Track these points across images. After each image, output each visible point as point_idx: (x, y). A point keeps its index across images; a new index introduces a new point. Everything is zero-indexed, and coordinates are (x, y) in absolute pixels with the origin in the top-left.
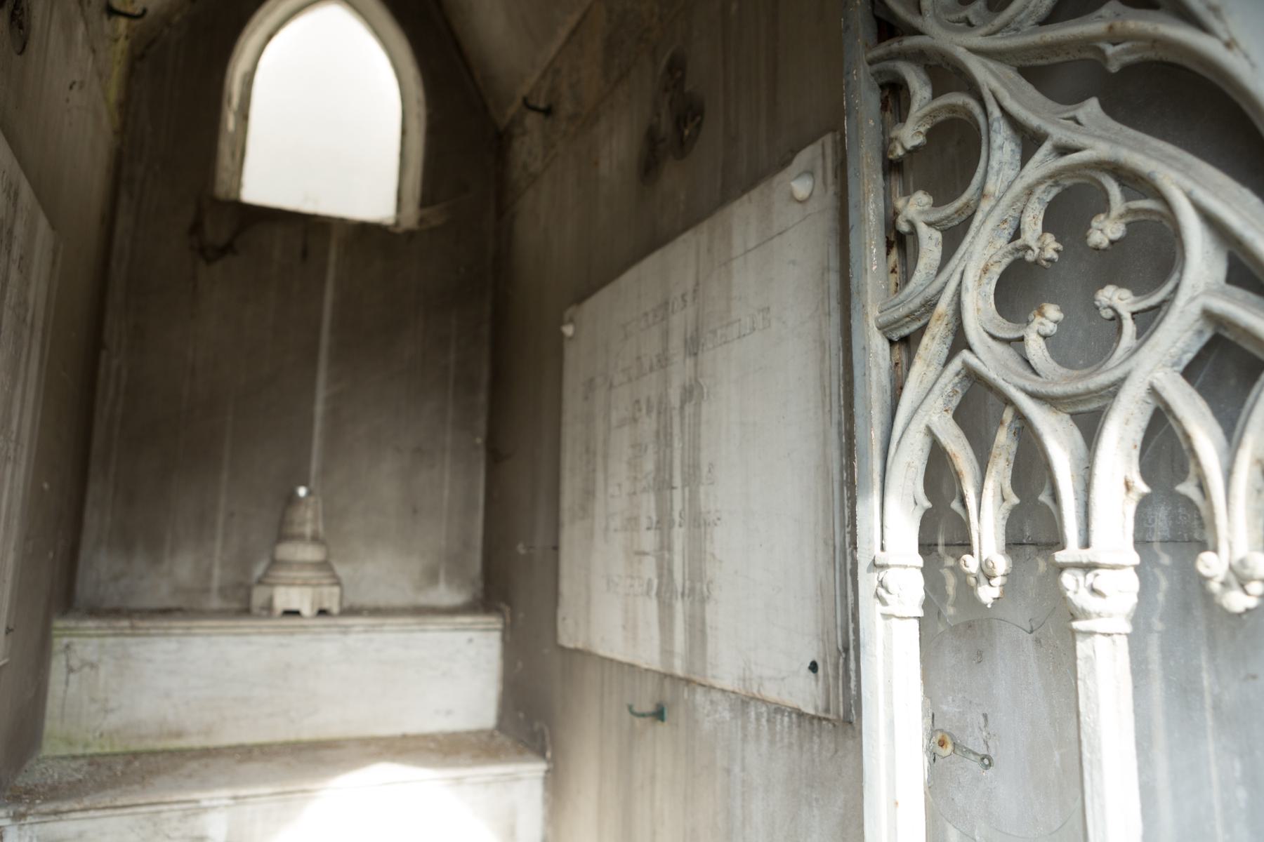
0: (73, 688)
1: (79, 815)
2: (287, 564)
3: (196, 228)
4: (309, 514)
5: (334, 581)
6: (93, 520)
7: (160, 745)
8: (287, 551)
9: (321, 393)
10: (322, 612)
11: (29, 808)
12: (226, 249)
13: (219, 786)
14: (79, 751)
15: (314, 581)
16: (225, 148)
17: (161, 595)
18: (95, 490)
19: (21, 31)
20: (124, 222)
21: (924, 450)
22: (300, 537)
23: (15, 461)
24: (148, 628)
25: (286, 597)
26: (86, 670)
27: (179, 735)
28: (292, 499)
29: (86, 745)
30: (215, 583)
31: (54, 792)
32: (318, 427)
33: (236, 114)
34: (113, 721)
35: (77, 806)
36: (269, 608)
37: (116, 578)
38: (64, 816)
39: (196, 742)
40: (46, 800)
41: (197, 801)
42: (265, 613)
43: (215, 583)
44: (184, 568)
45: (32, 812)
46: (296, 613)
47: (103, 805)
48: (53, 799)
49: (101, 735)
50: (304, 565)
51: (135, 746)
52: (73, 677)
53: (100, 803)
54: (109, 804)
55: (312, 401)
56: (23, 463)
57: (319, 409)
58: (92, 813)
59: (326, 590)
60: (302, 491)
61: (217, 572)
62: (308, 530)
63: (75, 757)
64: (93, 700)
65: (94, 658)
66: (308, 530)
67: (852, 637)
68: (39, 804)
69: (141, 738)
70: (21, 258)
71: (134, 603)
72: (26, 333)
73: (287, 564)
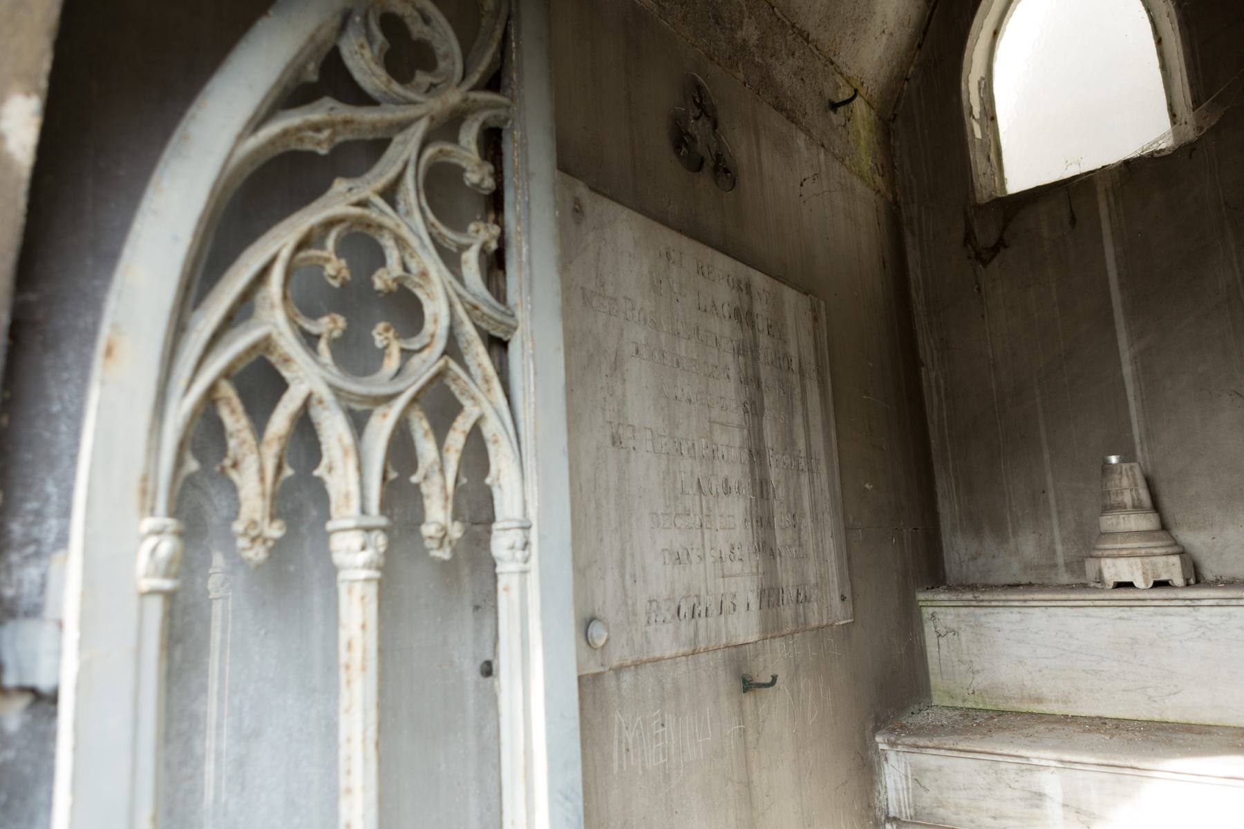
0: (944, 651)
1: (933, 751)
2: (1111, 535)
3: (969, 238)
4: (1125, 482)
5: (1176, 549)
6: (947, 510)
7: (1024, 708)
8: (1109, 522)
9: (1126, 354)
10: (1159, 584)
11: (897, 739)
12: (1000, 244)
13: (1045, 747)
14: (959, 704)
15: (1143, 552)
16: (977, 157)
17: (1014, 572)
18: (943, 485)
19: (729, 174)
20: (913, 257)
21: (465, 345)
22: (1121, 507)
23: (810, 471)
24: (990, 601)
25: (1116, 569)
26: (950, 635)
27: (1039, 700)
28: (1106, 469)
29: (964, 701)
30: (1060, 560)
31: (935, 730)
32: (1130, 390)
33: (980, 121)
34: (980, 681)
35: (929, 744)
36: (1100, 579)
37: (974, 559)
38: (924, 751)
39: (1058, 709)
40: (909, 735)
41: (1027, 758)
42: (1099, 585)
43: (1060, 560)
44: (1028, 546)
45: (899, 742)
46: (1129, 585)
47: (947, 746)
48: (915, 735)
49: (973, 693)
50: (1129, 534)
51: (1002, 706)
52: (942, 641)
53: (945, 744)
54: (952, 746)
55: (1119, 365)
56: (823, 468)
57: (1127, 370)
58: (942, 752)
59: (1161, 560)
60: (1114, 459)
61: (1059, 548)
62: (1127, 498)
63: (955, 708)
64: (961, 661)
65: (954, 626)
66: (1127, 498)
67: (771, 509)
68: (904, 737)
69: (1007, 699)
70: (769, 327)
71: (991, 581)
72: (795, 378)
73: (1111, 535)
